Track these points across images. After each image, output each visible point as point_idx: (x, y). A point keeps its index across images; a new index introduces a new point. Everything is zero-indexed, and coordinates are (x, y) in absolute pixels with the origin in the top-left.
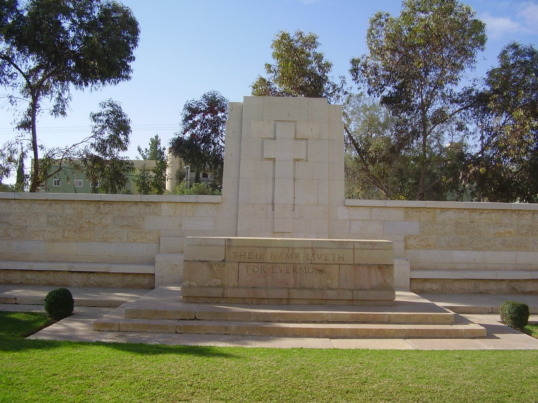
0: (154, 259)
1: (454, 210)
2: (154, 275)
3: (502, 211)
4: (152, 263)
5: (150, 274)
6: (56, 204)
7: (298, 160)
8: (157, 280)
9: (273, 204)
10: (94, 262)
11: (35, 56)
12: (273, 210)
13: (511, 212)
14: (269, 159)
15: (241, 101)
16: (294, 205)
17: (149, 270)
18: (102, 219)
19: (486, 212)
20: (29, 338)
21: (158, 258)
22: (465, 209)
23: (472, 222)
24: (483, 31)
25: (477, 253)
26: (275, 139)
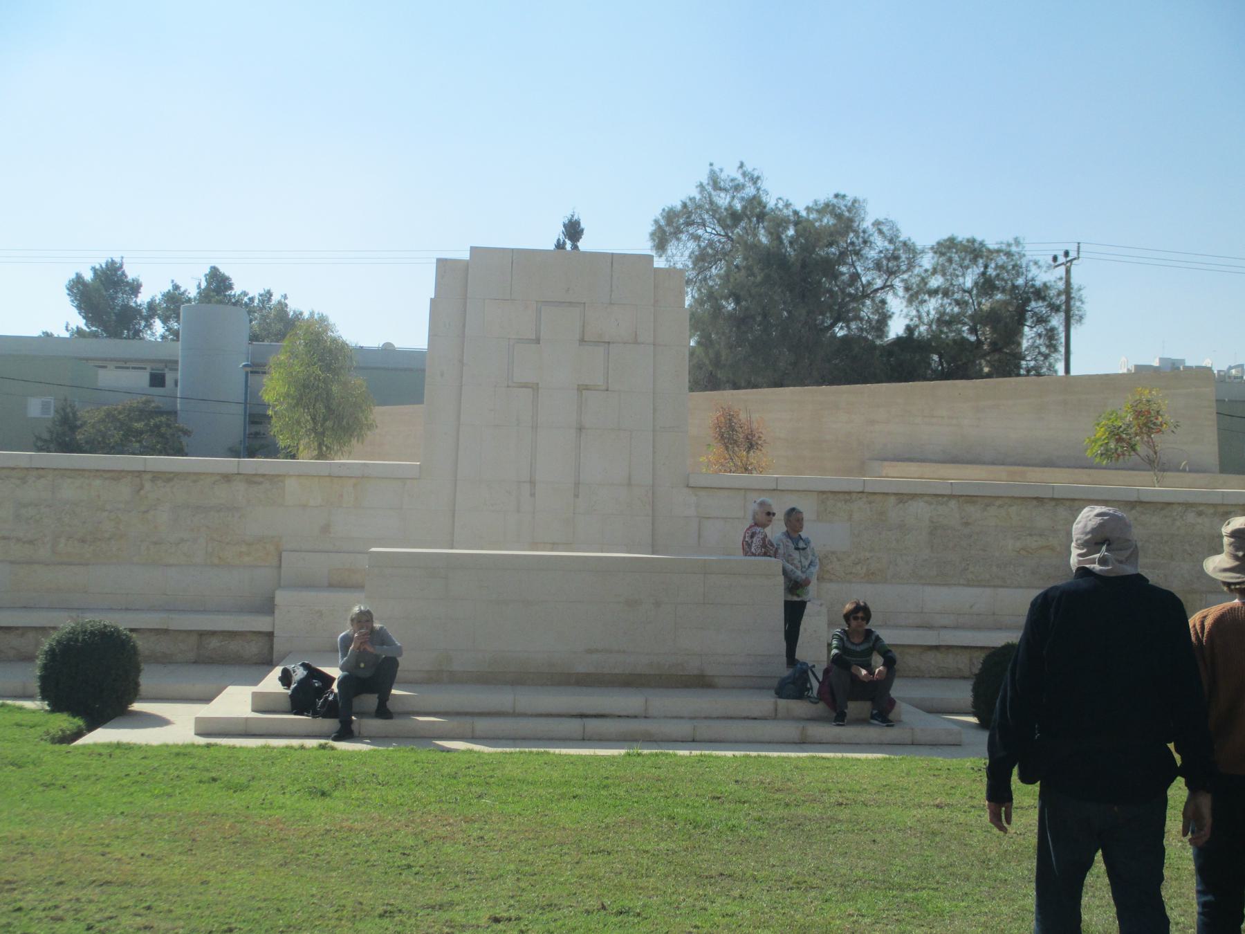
0: (272, 599)
1: (926, 498)
2: (270, 635)
3: (1035, 502)
4: (268, 607)
5: (260, 633)
6: (39, 477)
7: (587, 388)
8: (278, 646)
9: (532, 483)
10: (127, 609)
11: (330, 333)
12: (533, 495)
13: (1053, 503)
14: (525, 386)
15: (465, 255)
16: (577, 484)
17: (261, 623)
18: (147, 512)
19: (998, 502)
20: (80, 742)
21: (281, 597)
22: (951, 497)
23: (967, 524)
24: (890, 265)
25: (978, 591)
26: (538, 341)
